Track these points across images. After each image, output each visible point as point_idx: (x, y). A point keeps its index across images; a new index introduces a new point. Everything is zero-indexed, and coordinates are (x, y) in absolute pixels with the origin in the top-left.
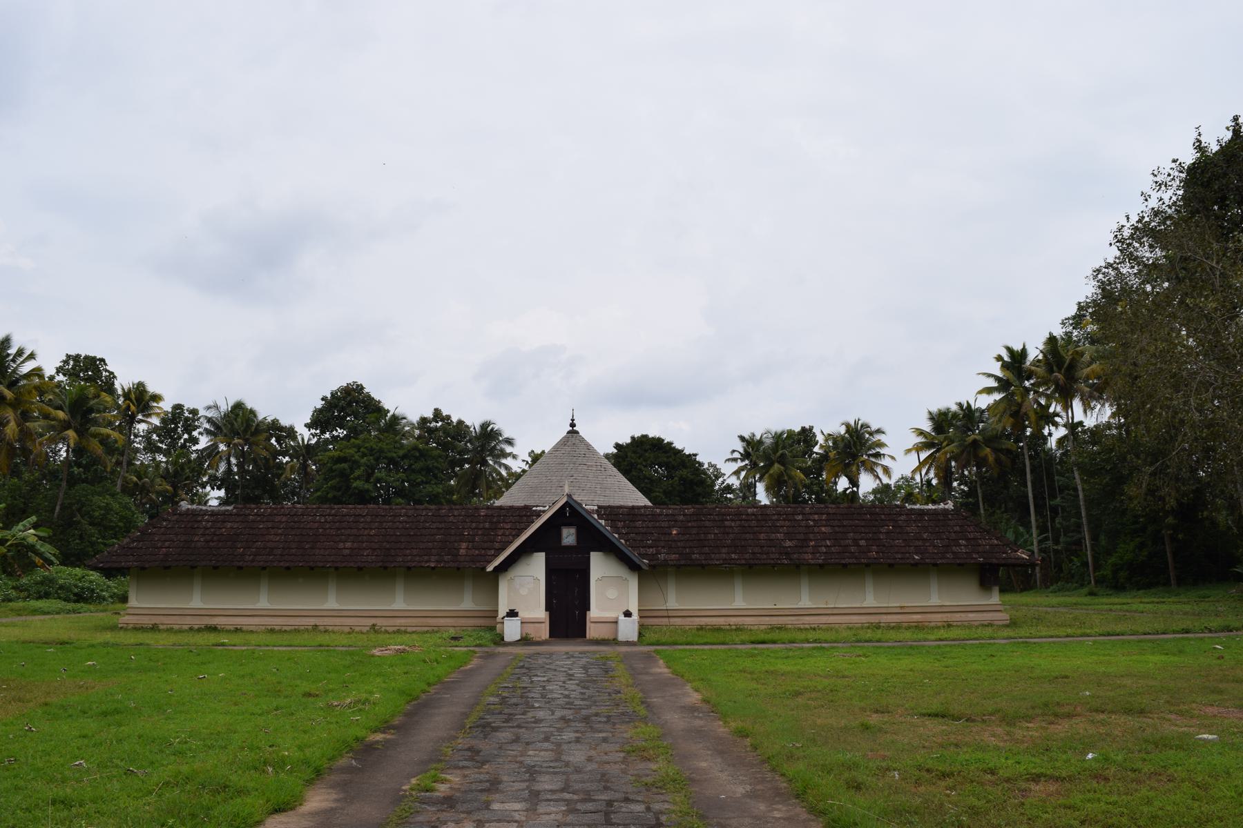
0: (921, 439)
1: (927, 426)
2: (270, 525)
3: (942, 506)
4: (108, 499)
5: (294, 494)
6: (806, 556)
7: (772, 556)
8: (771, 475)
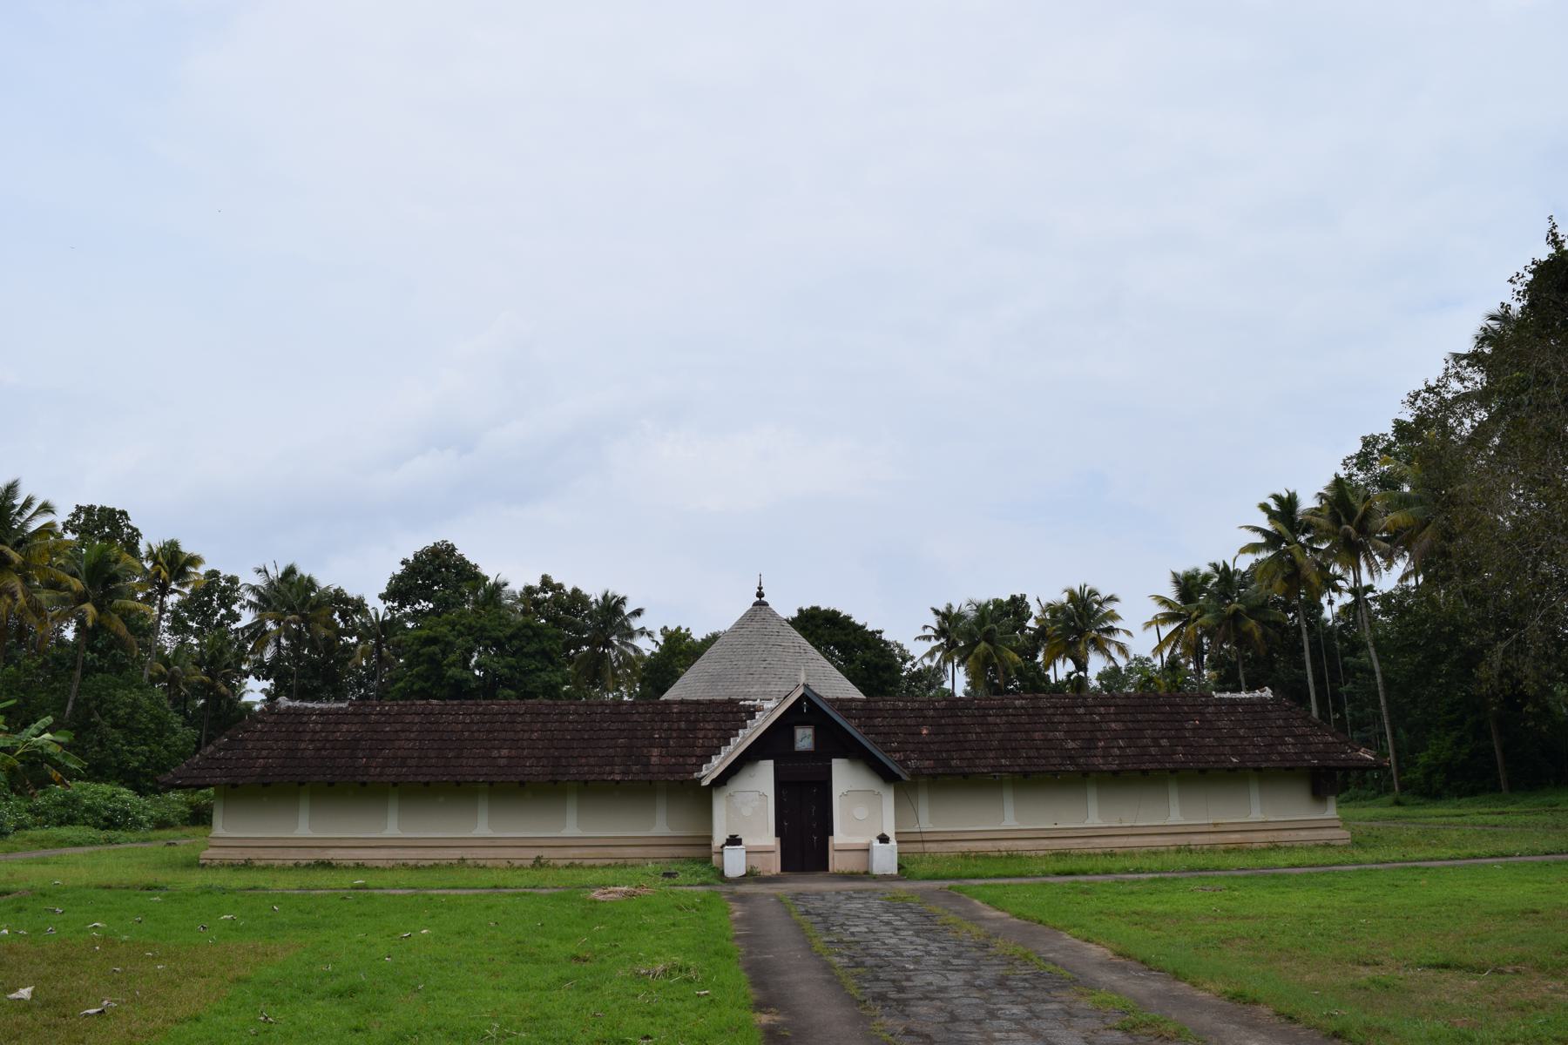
1: (1171, 593)
2: (398, 727)
3: (1258, 693)
5: (360, 685)
6: (1095, 761)
7: (1053, 761)
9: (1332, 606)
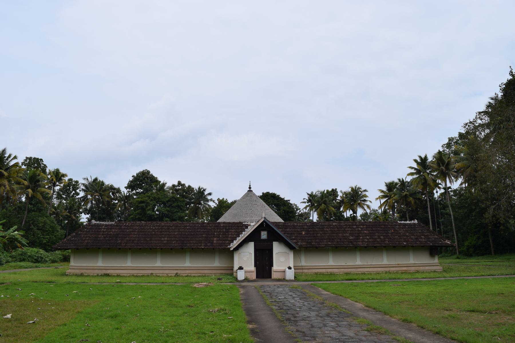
0: (382, 194)
1: (385, 189)
3: (413, 222)
4: (45, 219)
8: (321, 209)
9: (437, 193)
